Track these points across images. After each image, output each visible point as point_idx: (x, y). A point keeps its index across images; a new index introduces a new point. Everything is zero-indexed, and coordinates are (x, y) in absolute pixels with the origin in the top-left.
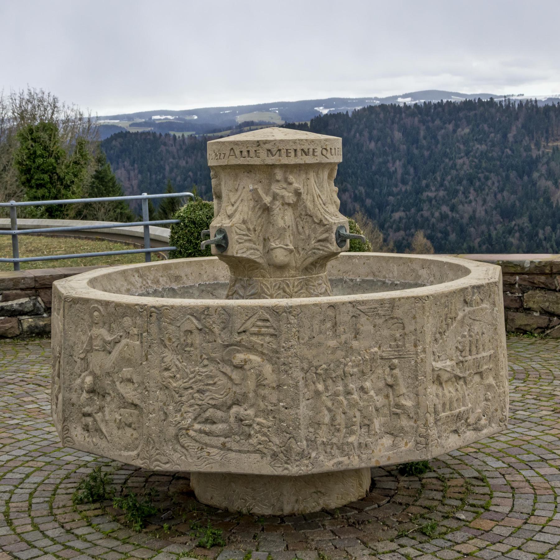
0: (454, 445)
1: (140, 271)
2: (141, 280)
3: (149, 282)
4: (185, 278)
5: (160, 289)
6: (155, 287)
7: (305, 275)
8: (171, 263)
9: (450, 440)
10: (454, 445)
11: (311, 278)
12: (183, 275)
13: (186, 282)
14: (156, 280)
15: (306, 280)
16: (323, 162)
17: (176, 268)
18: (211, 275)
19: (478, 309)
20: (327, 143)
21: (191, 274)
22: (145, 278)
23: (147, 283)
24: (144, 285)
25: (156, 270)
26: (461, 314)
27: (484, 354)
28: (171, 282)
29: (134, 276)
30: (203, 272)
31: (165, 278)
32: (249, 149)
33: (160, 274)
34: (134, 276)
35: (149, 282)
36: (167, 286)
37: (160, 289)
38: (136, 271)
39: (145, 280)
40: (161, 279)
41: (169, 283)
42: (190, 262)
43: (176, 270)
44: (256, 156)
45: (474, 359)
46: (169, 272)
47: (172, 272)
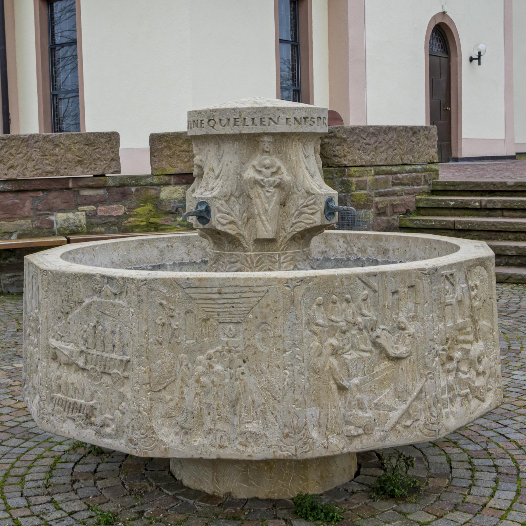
0: (67, 432)
1: (348, 237)
2: (345, 246)
3: (355, 250)
4: (391, 252)
5: (364, 259)
6: (360, 255)
7: (219, 250)
8: (383, 235)
9: (64, 425)
10: (67, 432)
11: (223, 254)
12: (391, 249)
13: (391, 256)
14: (363, 249)
15: (219, 254)
16: (210, 133)
17: (386, 240)
18: (413, 254)
19: (107, 302)
20: (215, 114)
21: (398, 249)
22: (352, 244)
23: (353, 250)
24: (348, 252)
25: (367, 239)
26: (87, 301)
27: (114, 356)
28: (378, 254)
29: (338, 241)
30: (408, 250)
31: (373, 249)
32: (255, 116)
33: (370, 244)
34: (338, 241)
35: (355, 250)
36: (373, 257)
37: (364, 259)
38: (342, 237)
39: (351, 247)
40: (369, 249)
41: (376, 254)
42: (400, 237)
43: (386, 243)
44: (261, 124)
45: (98, 355)
46: (379, 243)
47: (382, 244)
